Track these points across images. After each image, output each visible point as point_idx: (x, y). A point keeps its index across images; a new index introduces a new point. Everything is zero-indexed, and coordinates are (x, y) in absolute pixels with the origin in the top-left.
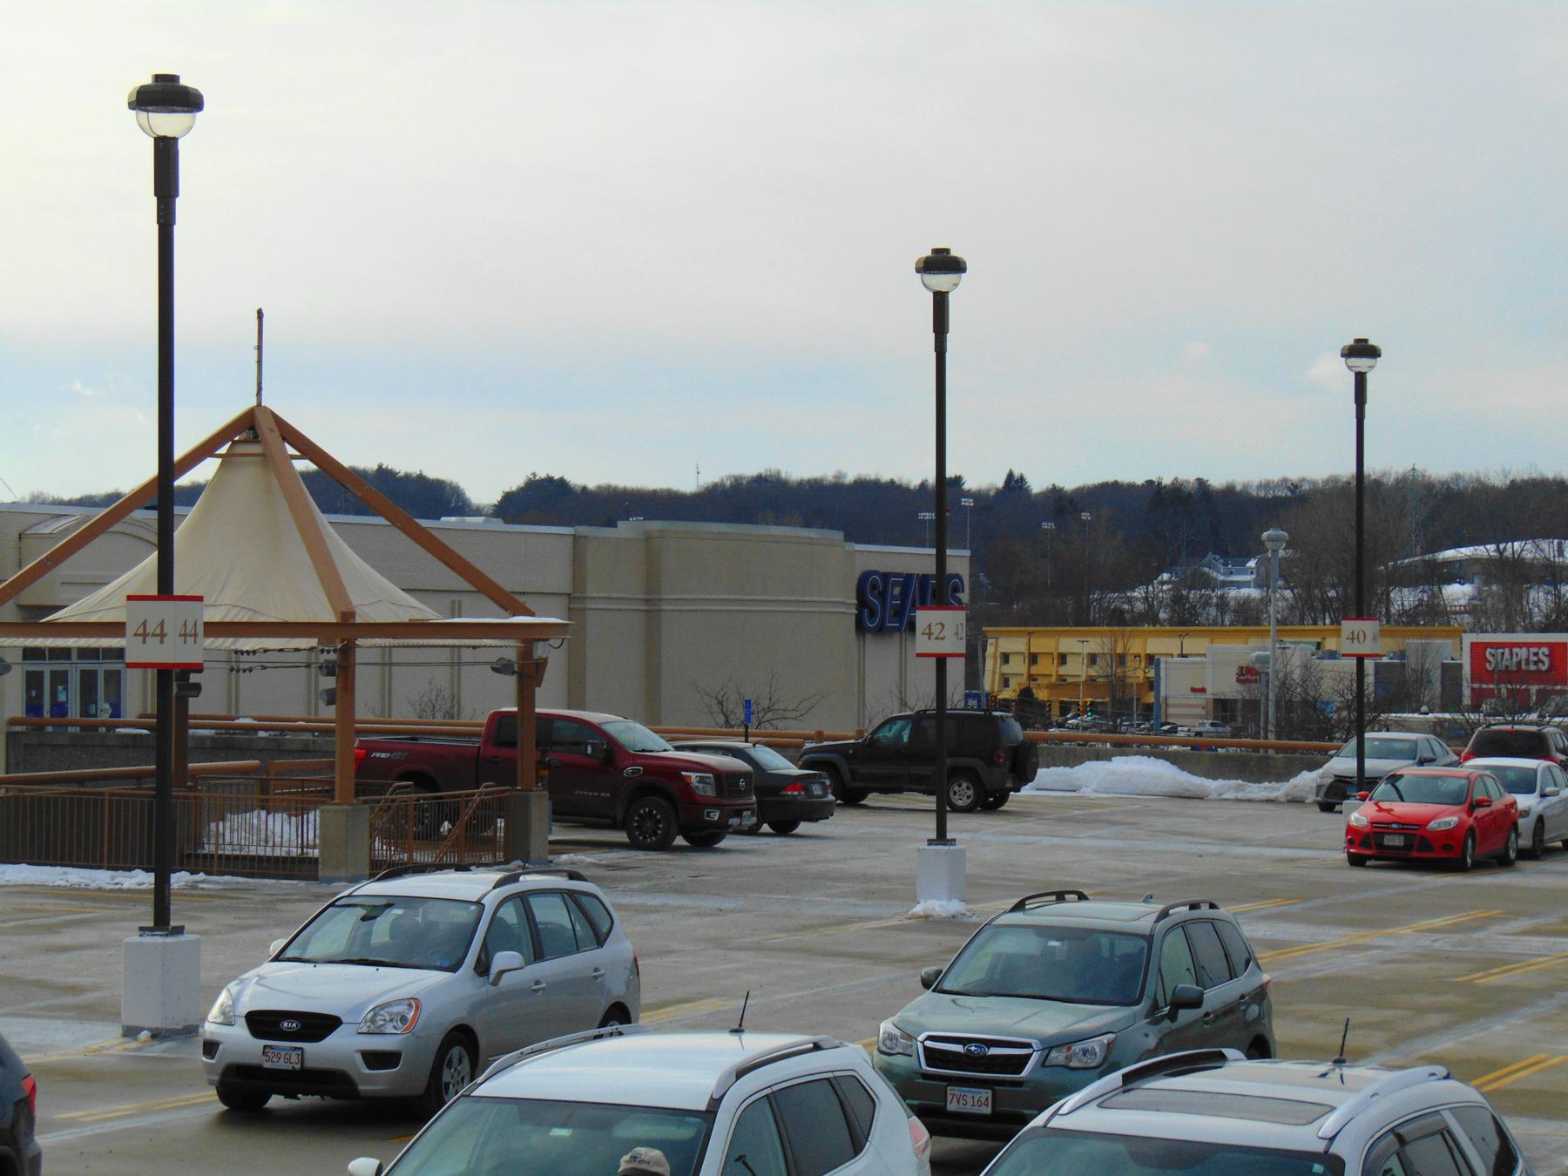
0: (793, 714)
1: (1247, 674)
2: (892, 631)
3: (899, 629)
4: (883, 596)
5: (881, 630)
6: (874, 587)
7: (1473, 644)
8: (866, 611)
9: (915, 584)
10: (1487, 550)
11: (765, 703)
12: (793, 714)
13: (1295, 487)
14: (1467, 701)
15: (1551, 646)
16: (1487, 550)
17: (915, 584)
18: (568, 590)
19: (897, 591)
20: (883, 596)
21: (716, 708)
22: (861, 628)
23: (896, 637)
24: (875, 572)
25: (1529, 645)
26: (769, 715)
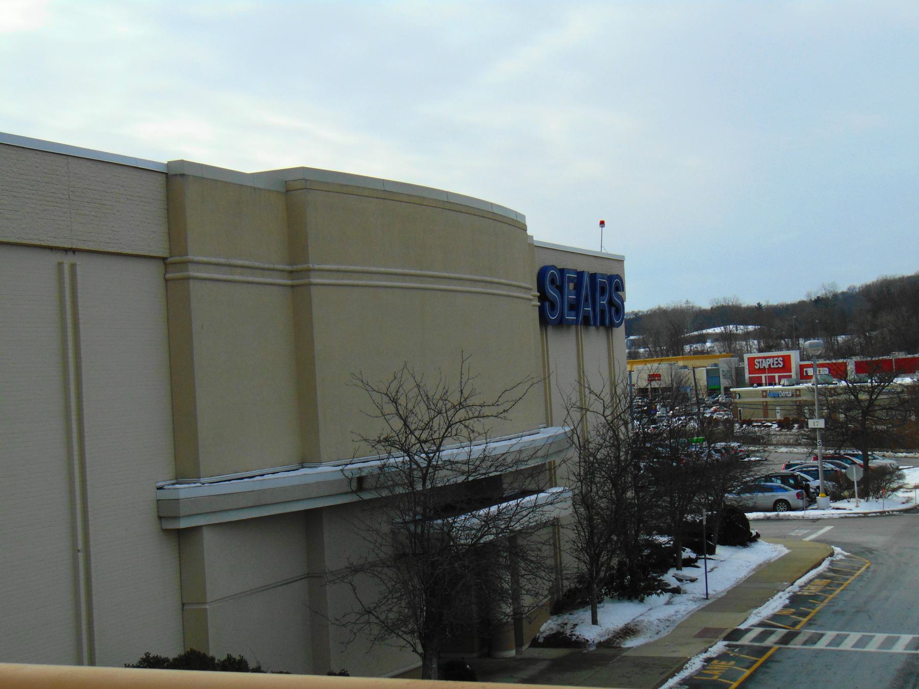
0: (494, 410)
1: (653, 377)
2: (569, 324)
3: (576, 322)
4: (560, 289)
5: (561, 323)
6: (553, 281)
7: (749, 359)
8: (547, 304)
9: (586, 280)
10: (718, 330)
11: (455, 398)
12: (494, 410)
13: (636, 314)
14: (777, 381)
15: (783, 357)
16: (718, 330)
17: (586, 280)
18: (159, 249)
19: (572, 286)
20: (560, 289)
21: (390, 408)
22: (544, 321)
23: (573, 328)
24: (553, 267)
25: (773, 357)
26: (462, 414)
